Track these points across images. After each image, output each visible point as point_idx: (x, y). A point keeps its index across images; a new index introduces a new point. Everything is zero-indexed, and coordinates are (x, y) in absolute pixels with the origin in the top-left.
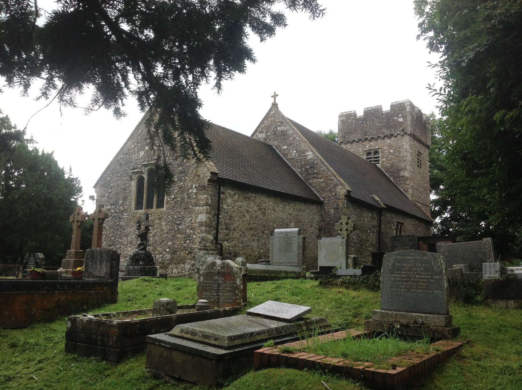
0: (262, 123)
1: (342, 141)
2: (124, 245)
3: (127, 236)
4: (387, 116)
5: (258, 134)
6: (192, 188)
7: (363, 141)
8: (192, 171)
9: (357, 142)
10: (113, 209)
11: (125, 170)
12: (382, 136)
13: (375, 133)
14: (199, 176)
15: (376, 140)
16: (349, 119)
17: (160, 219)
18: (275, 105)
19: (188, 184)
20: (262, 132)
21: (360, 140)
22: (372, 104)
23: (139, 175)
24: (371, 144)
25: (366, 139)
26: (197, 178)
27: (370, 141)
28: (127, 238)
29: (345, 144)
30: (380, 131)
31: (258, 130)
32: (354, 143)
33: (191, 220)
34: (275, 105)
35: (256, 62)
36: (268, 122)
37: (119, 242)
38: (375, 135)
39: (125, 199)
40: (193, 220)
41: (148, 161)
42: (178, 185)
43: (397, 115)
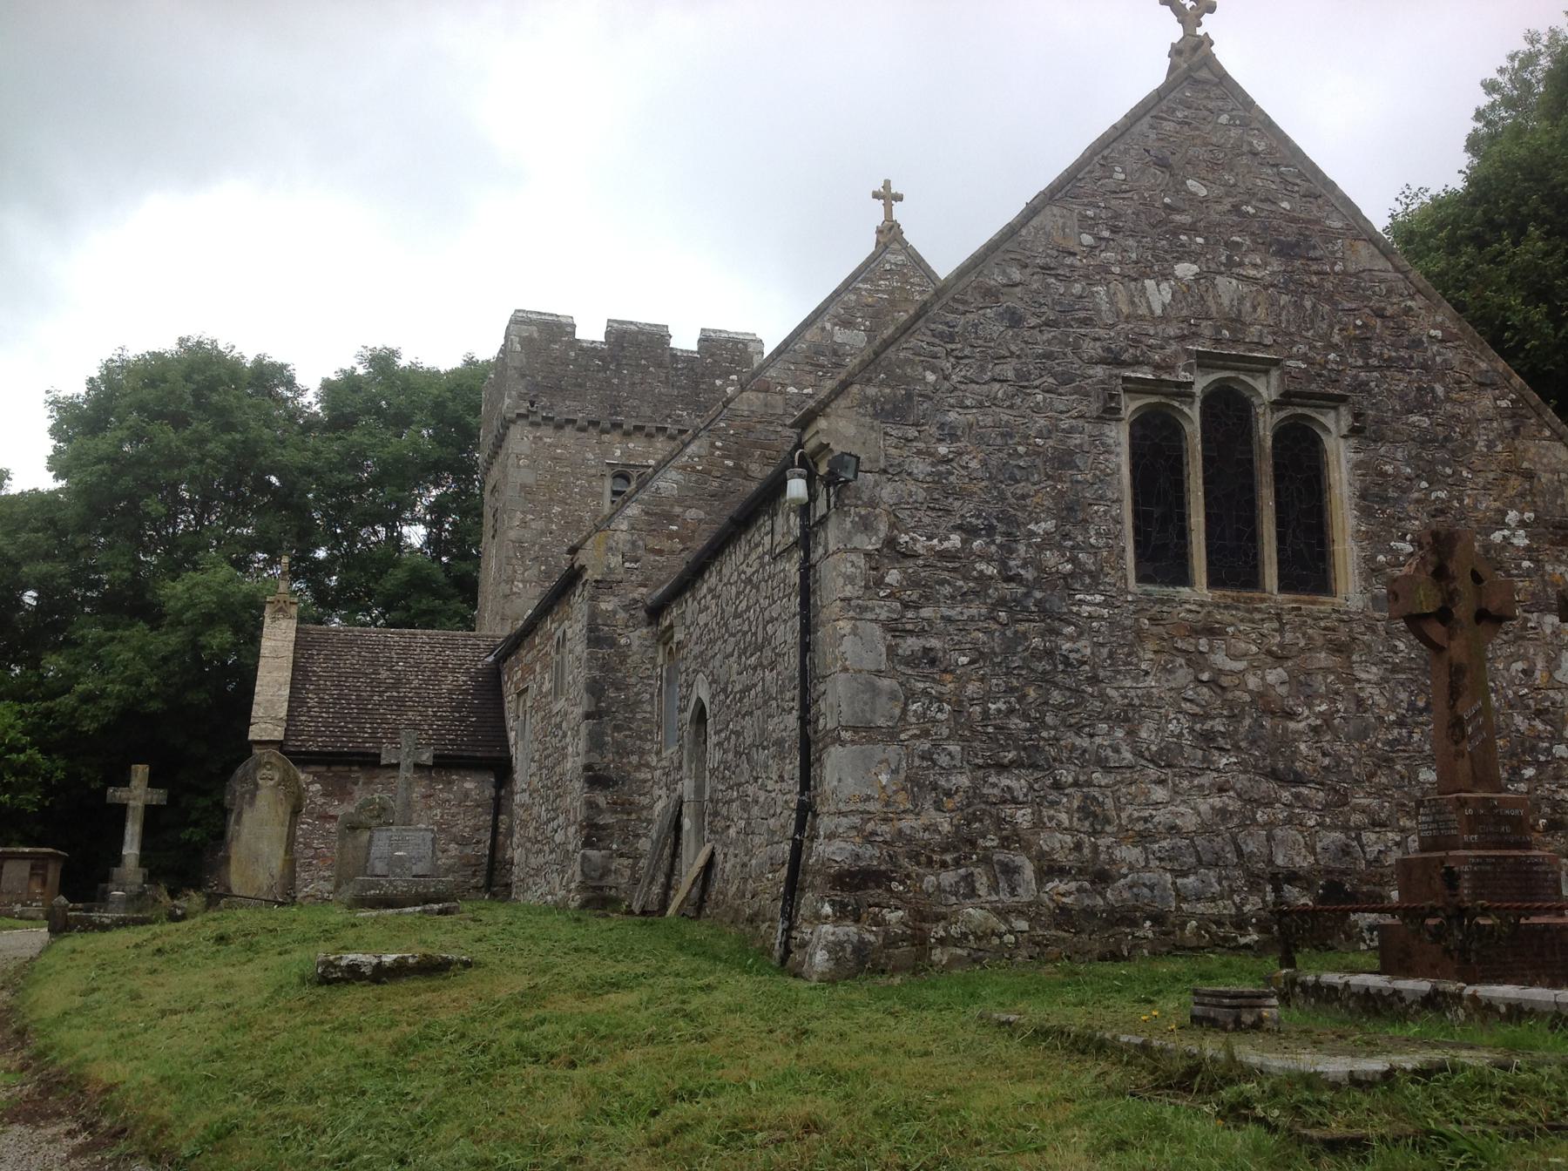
0: (847, 285)
1: (523, 411)
2: (1108, 770)
3: (1127, 720)
4: (692, 369)
5: (828, 326)
6: (1502, 525)
7: (604, 431)
8: (1490, 445)
9: (582, 429)
10: (988, 559)
11: (1049, 356)
12: (672, 429)
13: (649, 413)
14: (1529, 475)
15: (650, 436)
16: (555, 343)
17: (1338, 648)
18: (890, 234)
19: (1476, 501)
20: (847, 324)
21: (594, 424)
22: (641, 313)
23: (1154, 399)
24: (631, 445)
25: (616, 426)
26: (1515, 484)
27: (627, 434)
28: (1131, 733)
29: (533, 424)
30: (667, 412)
31: (832, 311)
32: (568, 429)
33: (1524, 671)
34: (890, 234)
35: (1482, 91)
36: (878, 291)
37: (1073, 748)
38: (651, 419)
39: (1070, 511)
40: (1539, 676)
41: (1218, 341)
42: (1416, 495)
43: (725, 375)
